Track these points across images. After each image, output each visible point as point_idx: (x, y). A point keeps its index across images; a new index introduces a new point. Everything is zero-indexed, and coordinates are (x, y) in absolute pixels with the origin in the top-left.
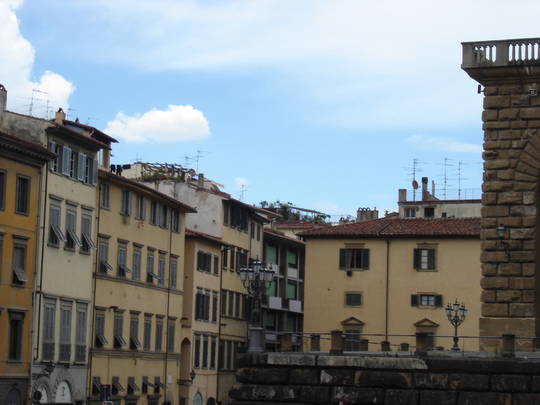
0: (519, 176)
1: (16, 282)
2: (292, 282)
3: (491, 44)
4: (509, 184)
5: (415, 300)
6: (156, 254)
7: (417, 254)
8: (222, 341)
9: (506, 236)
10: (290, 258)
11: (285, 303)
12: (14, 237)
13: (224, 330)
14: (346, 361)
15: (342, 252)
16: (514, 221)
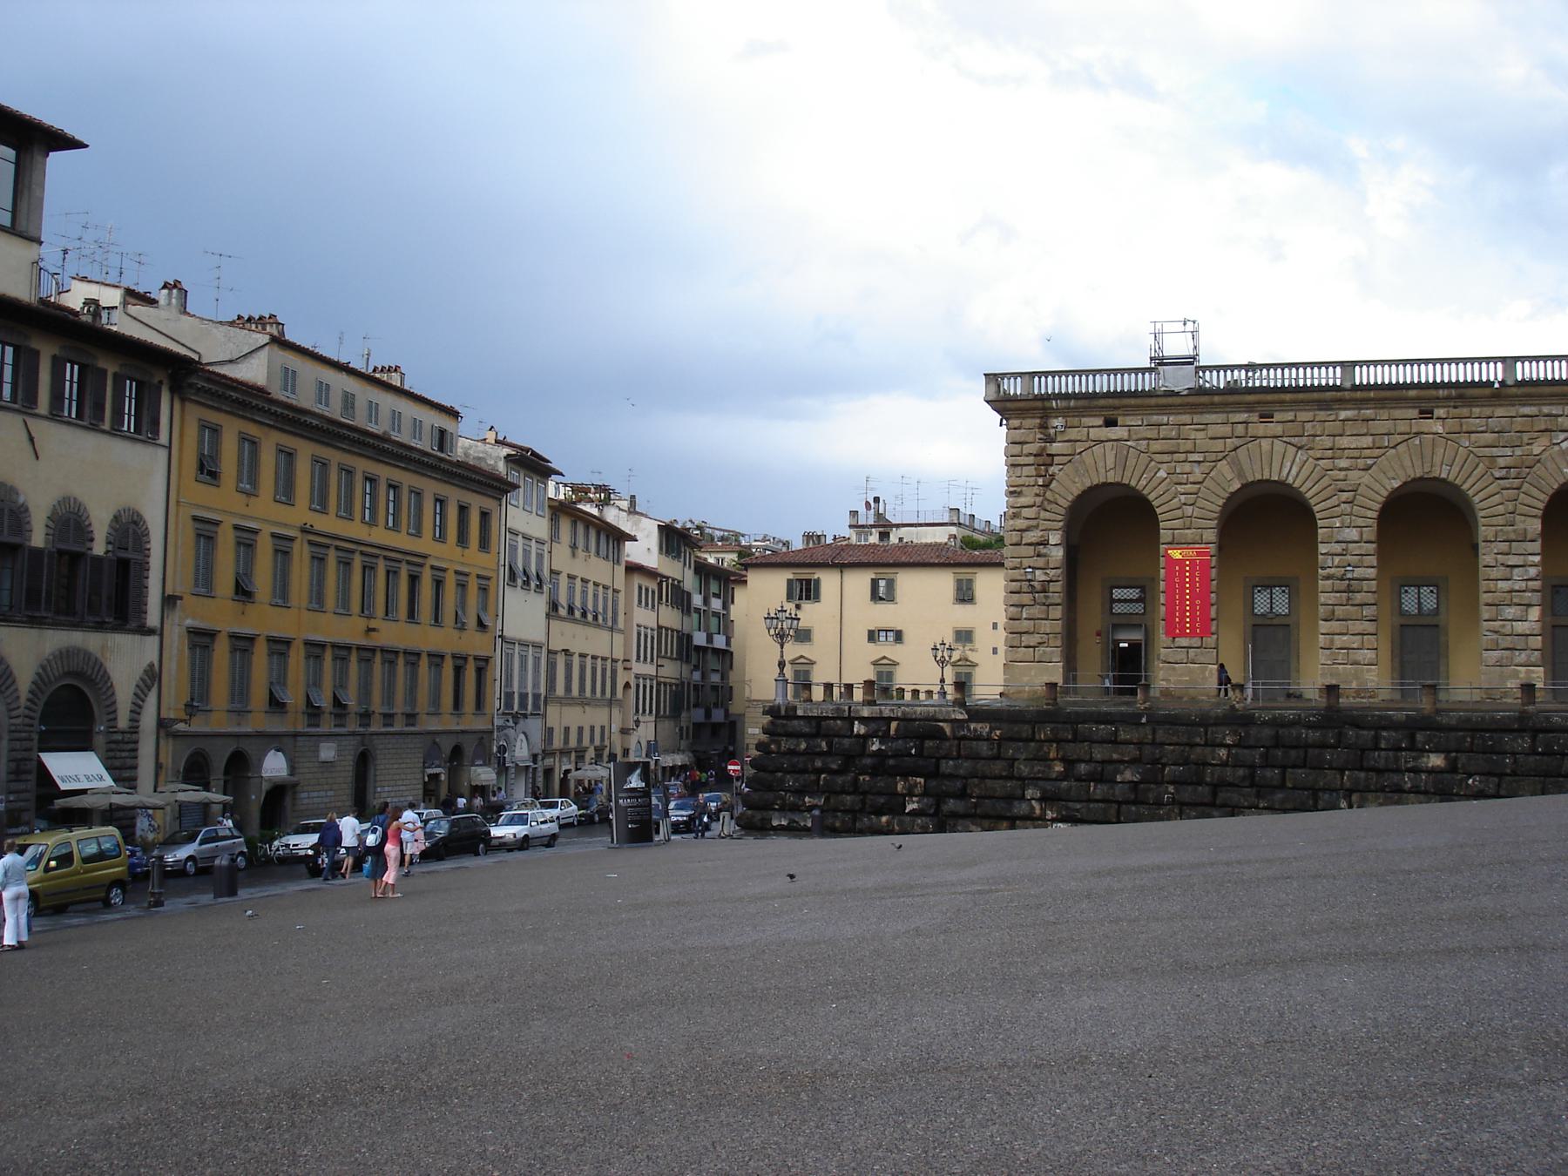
1: (481, 625)
2: (716, 614)
4: (1034, 523)
5: (872, 636)
6: (578, 582)
7: (875, 583)
8: (658, 684)
10: (714, 588)
11: (710, 639)
12: (478, 577)
13: (662, 671)
15: (790, 582)
16: (1040, 562)
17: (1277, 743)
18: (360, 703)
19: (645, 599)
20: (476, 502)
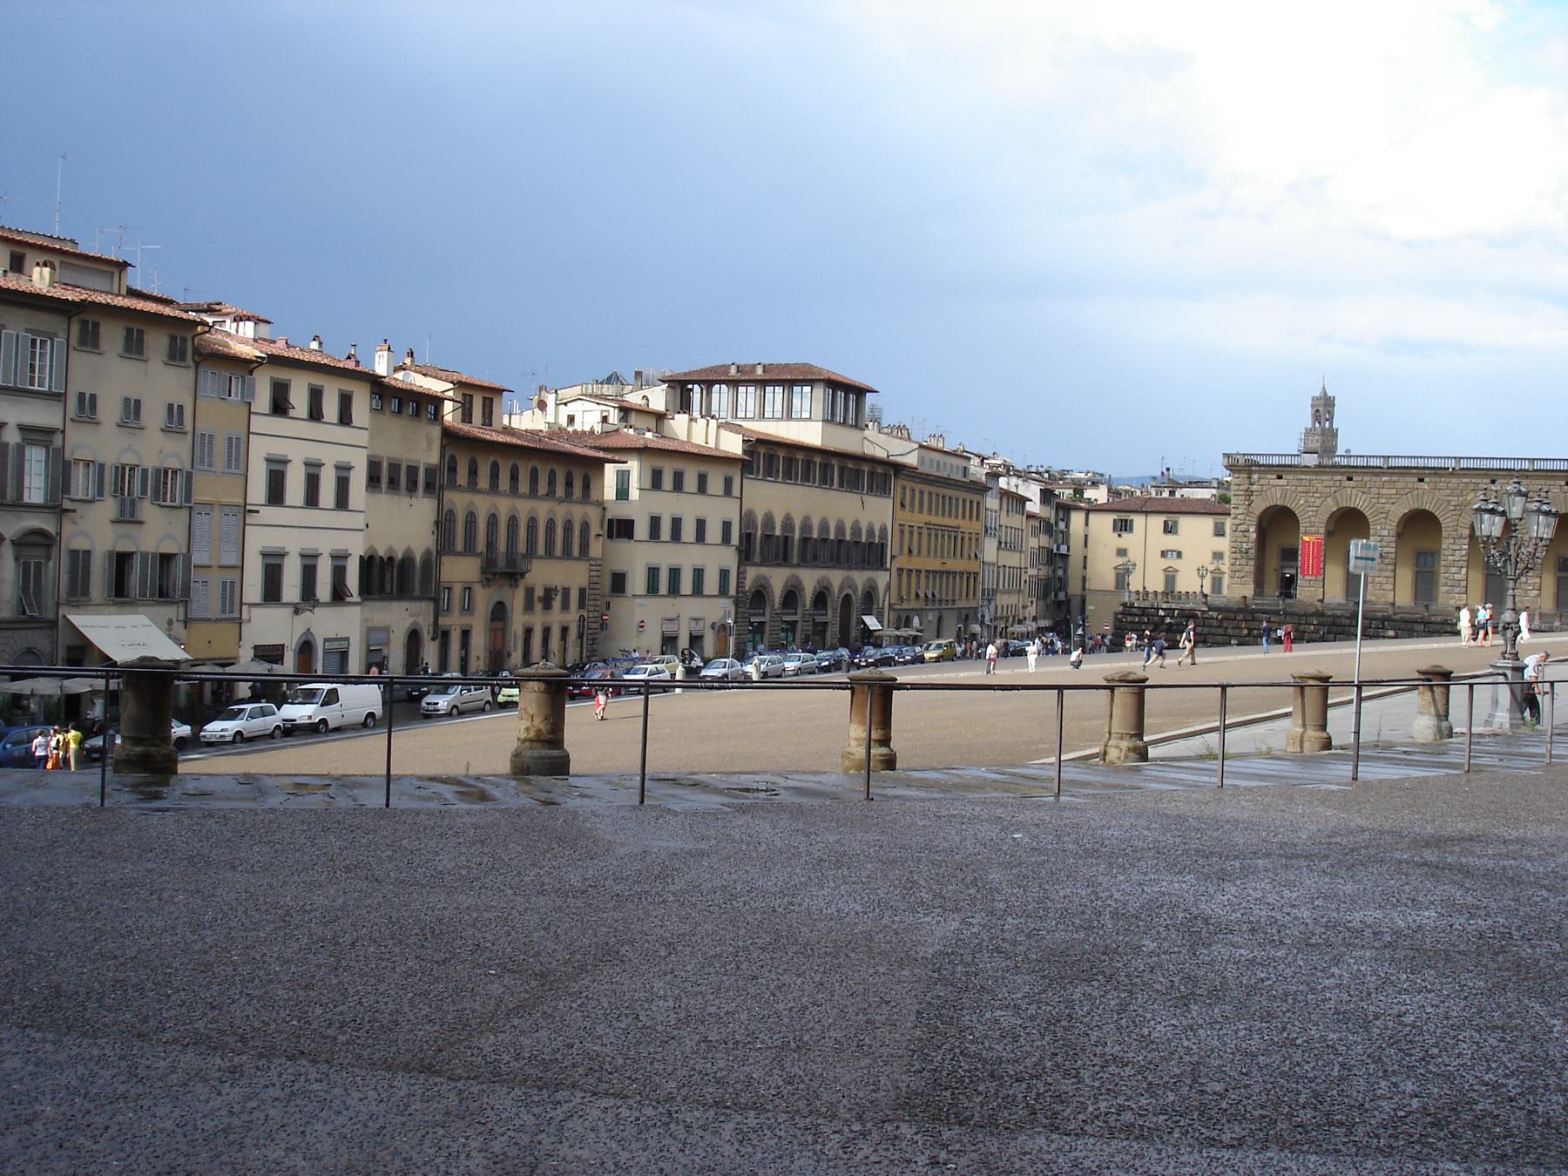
5: (1164, 554)
17: (1334, 624)
19: (1035, 532)
20: (975, 498)
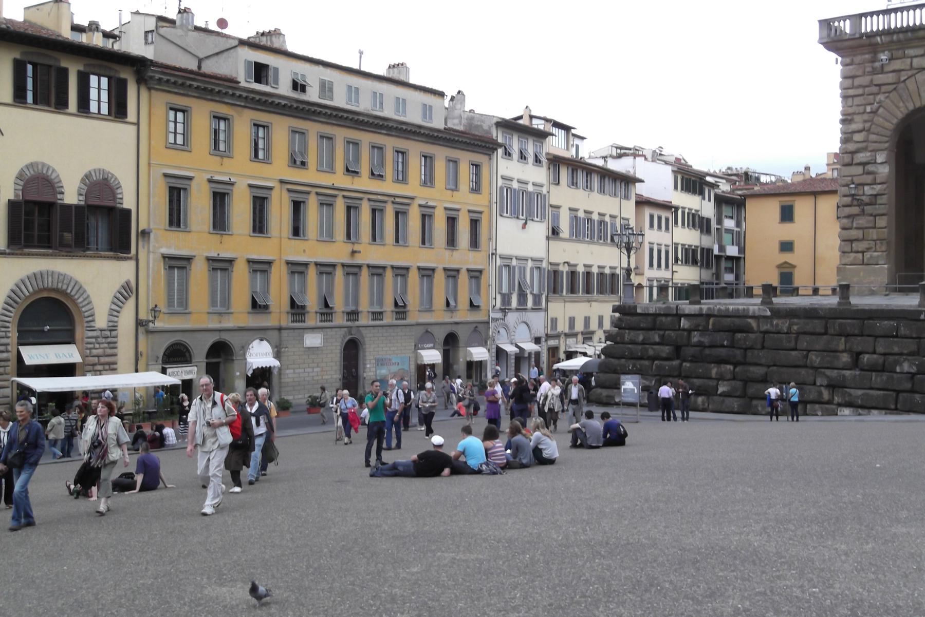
0: (873, 137)
3: (844, 18)
4: (864, 145)
9: (861, 192)
14: (701, 309)
16: (869, 178)
18: (347, 303)
